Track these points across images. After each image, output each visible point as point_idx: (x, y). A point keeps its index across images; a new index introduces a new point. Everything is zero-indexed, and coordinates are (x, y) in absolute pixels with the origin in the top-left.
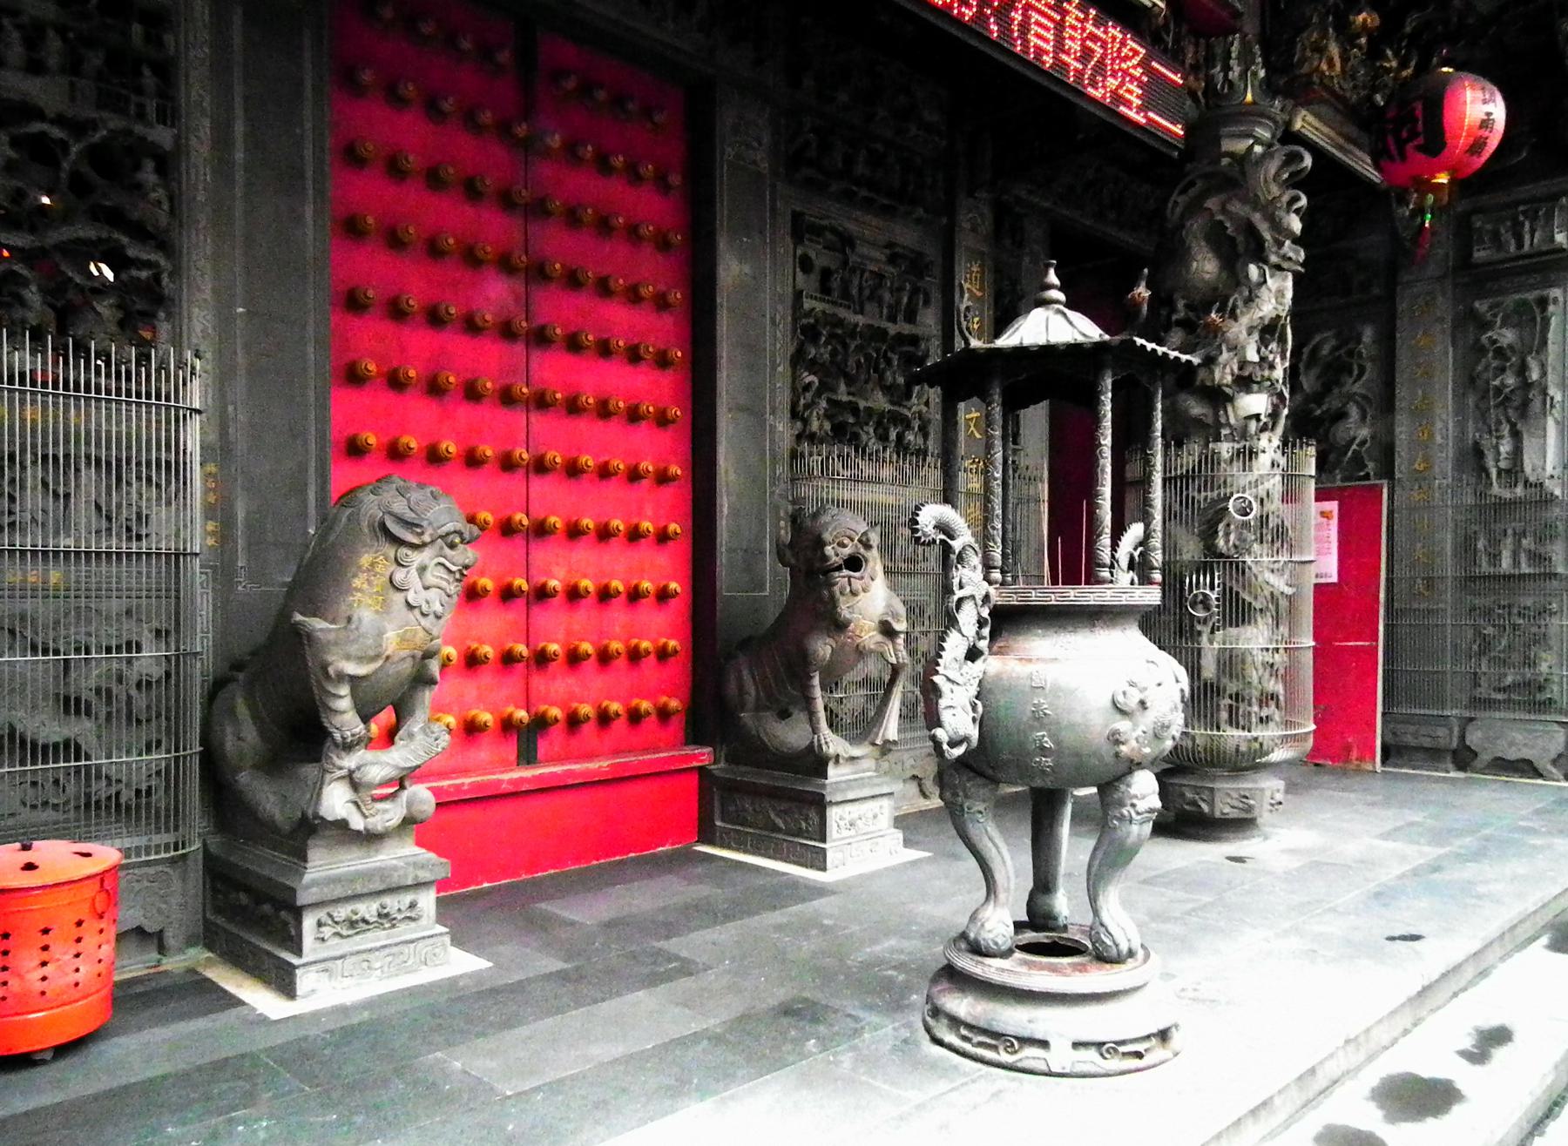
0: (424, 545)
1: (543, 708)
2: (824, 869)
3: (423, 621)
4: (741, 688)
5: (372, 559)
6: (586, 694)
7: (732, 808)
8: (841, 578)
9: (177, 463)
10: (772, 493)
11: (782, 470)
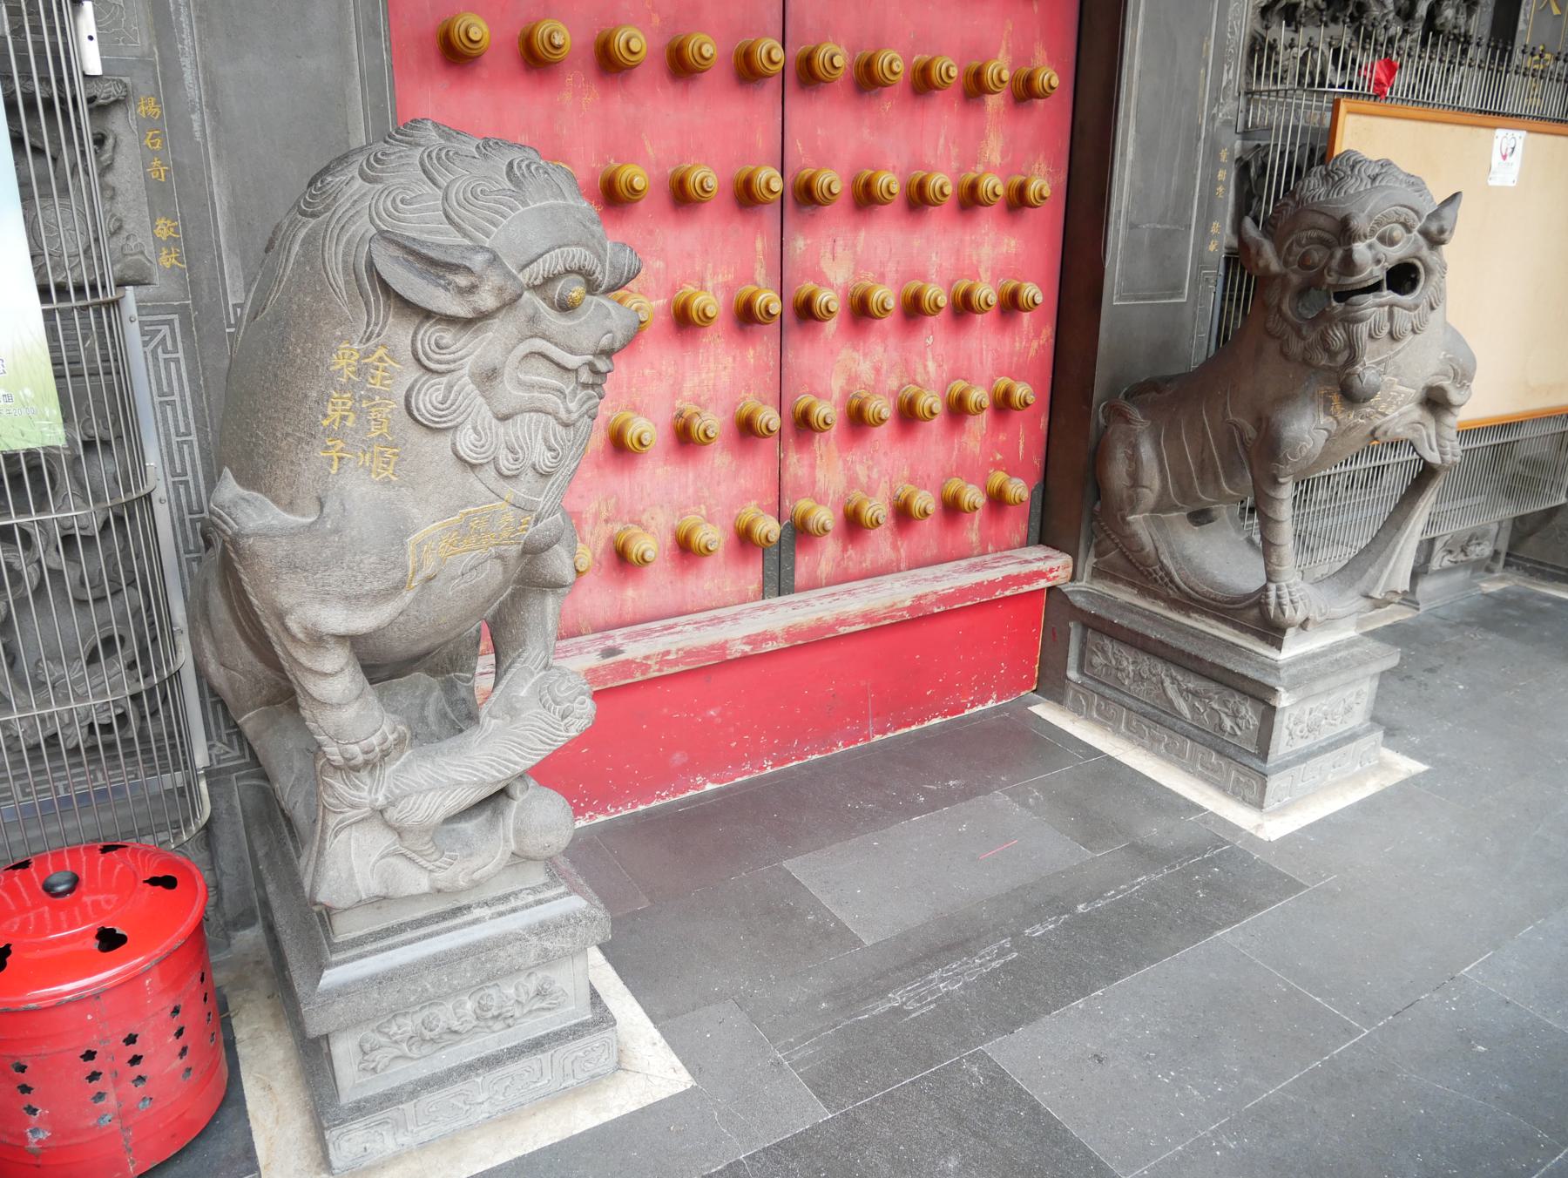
0: (480, 318)
1: (804, 504)
2: (1259, 805)
3: (510, 491)
4: (1135, 480)
5: (366, 365)
6: (878, 473)
7: (1098, 660)
8: (1372, 308)
9: (63, 101)
10: (1213, 118)
11: (1233, 75)
